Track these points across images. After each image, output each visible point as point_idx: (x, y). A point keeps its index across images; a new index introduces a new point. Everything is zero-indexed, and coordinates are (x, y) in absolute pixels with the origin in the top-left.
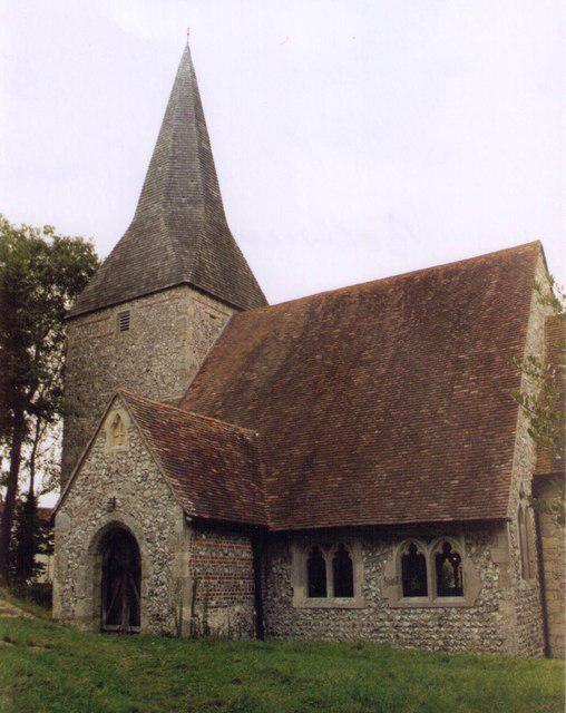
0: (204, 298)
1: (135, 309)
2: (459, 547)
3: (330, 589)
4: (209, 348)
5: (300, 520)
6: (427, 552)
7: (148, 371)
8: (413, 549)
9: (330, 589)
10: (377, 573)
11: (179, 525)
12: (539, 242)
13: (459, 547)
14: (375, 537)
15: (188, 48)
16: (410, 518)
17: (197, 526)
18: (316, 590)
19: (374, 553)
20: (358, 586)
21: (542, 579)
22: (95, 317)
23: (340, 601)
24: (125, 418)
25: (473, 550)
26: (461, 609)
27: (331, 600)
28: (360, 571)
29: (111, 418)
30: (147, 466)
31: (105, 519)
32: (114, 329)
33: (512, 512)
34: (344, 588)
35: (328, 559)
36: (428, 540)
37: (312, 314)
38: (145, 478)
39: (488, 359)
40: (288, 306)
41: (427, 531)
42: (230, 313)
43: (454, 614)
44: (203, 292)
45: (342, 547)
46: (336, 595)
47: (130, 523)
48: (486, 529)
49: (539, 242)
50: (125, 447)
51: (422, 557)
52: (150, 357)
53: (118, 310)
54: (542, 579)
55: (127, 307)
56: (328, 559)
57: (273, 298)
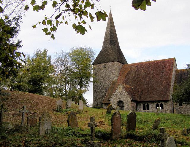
0: (119, 63)
1: (107, 64)
2: (163, 103)
3: (146, 109)
4: (120, 71)
5: (142, 100)
6: (159, 104)
8: (157, 104)
9: (146, 109)
10: (152, 107)
11: (130, 100)
12: (174, 59)
13: (163, 103)
14: (152, 102)
15: (110, 11)
16: (157, 100)
17: (132, 101)
18: (144, 109)
20: (150, 108)
21: (173, 108)
22: (98, 65)
23: (148, 110)
24: (121, 87)
26: (163, 111)
27: (146, 110)
28: (150, 106)
29: (119, 87)
30: (125, 93)
31: (119, 100)
32: (103, 67)
33: (170, 100)
34: (148, 108)
35: (146, 105)
36: (159, 103)
37: (137, 66)
38: (125, 94)
39: (167, 78)
40: (133, 64)
41: (159, 101)
42: (122, 64)
43: (162, 112)
44: (119, 62)
45: (148, 104)
46: (147, 109)
47: (122, 100)
48: (166, 101)
49: (174, 59)
50: (121, 91)
51: (158, 105)
53: (103, 64)
54: (173, 108)
55: (105, 64)
56: (146, 105)
57: (129, 62)
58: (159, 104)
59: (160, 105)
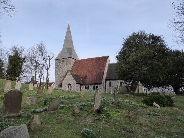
33: (102, 83)
42: (75, 60)
48: (100, 84)
58: (96, 86)
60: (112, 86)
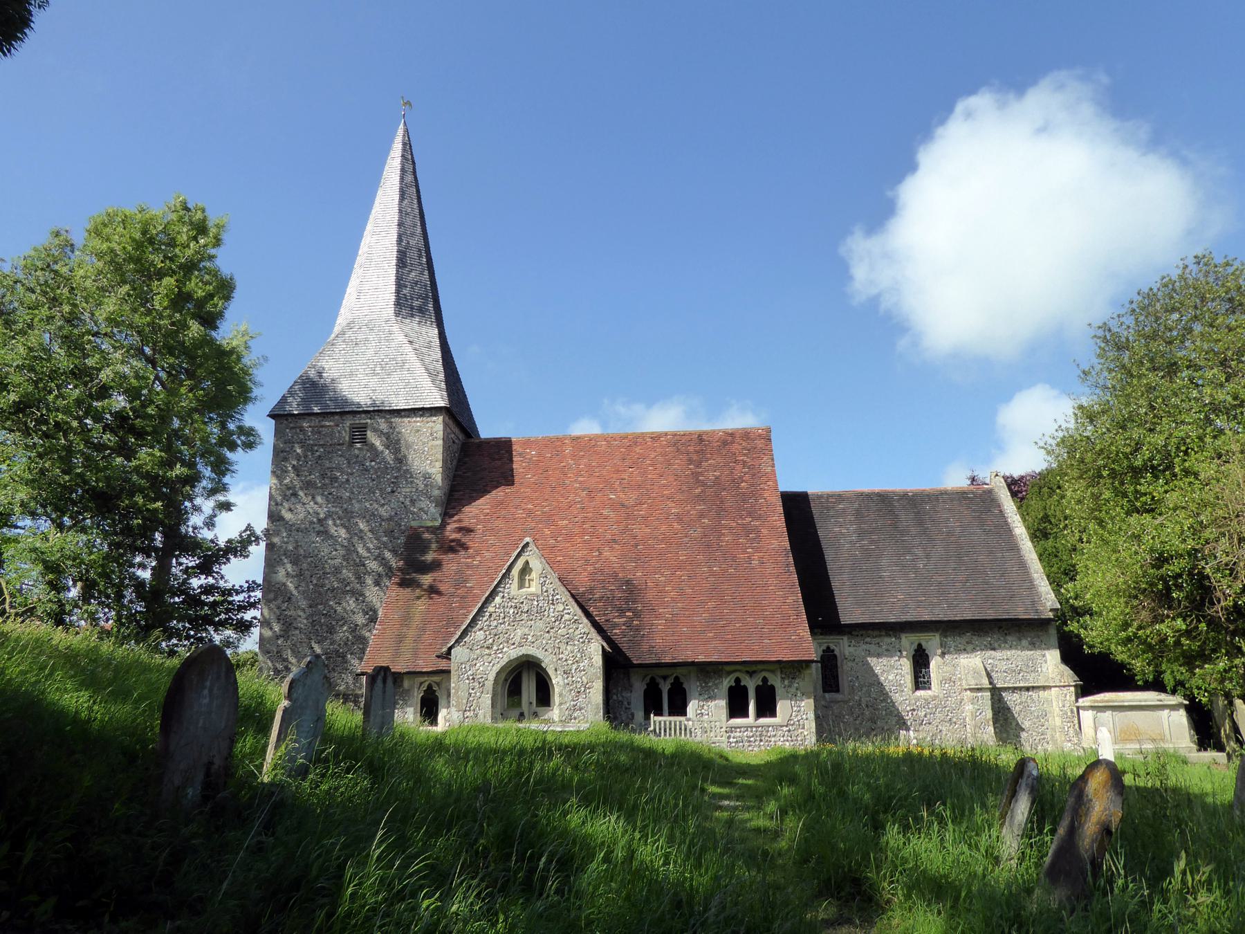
6: (751, 685)
7: (393, 492)
13: (775, 680)
19: (706, 683)
25: (786, 682)
41: (751, 667)
46: (670, 714)
52: (396, 478)
59: (758, 689)
60: (844, 681)
